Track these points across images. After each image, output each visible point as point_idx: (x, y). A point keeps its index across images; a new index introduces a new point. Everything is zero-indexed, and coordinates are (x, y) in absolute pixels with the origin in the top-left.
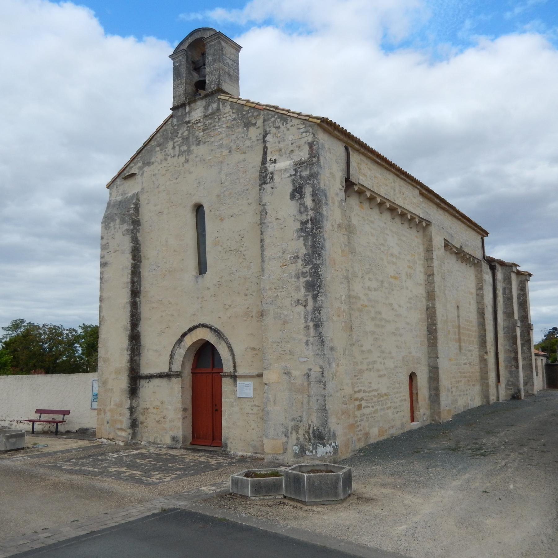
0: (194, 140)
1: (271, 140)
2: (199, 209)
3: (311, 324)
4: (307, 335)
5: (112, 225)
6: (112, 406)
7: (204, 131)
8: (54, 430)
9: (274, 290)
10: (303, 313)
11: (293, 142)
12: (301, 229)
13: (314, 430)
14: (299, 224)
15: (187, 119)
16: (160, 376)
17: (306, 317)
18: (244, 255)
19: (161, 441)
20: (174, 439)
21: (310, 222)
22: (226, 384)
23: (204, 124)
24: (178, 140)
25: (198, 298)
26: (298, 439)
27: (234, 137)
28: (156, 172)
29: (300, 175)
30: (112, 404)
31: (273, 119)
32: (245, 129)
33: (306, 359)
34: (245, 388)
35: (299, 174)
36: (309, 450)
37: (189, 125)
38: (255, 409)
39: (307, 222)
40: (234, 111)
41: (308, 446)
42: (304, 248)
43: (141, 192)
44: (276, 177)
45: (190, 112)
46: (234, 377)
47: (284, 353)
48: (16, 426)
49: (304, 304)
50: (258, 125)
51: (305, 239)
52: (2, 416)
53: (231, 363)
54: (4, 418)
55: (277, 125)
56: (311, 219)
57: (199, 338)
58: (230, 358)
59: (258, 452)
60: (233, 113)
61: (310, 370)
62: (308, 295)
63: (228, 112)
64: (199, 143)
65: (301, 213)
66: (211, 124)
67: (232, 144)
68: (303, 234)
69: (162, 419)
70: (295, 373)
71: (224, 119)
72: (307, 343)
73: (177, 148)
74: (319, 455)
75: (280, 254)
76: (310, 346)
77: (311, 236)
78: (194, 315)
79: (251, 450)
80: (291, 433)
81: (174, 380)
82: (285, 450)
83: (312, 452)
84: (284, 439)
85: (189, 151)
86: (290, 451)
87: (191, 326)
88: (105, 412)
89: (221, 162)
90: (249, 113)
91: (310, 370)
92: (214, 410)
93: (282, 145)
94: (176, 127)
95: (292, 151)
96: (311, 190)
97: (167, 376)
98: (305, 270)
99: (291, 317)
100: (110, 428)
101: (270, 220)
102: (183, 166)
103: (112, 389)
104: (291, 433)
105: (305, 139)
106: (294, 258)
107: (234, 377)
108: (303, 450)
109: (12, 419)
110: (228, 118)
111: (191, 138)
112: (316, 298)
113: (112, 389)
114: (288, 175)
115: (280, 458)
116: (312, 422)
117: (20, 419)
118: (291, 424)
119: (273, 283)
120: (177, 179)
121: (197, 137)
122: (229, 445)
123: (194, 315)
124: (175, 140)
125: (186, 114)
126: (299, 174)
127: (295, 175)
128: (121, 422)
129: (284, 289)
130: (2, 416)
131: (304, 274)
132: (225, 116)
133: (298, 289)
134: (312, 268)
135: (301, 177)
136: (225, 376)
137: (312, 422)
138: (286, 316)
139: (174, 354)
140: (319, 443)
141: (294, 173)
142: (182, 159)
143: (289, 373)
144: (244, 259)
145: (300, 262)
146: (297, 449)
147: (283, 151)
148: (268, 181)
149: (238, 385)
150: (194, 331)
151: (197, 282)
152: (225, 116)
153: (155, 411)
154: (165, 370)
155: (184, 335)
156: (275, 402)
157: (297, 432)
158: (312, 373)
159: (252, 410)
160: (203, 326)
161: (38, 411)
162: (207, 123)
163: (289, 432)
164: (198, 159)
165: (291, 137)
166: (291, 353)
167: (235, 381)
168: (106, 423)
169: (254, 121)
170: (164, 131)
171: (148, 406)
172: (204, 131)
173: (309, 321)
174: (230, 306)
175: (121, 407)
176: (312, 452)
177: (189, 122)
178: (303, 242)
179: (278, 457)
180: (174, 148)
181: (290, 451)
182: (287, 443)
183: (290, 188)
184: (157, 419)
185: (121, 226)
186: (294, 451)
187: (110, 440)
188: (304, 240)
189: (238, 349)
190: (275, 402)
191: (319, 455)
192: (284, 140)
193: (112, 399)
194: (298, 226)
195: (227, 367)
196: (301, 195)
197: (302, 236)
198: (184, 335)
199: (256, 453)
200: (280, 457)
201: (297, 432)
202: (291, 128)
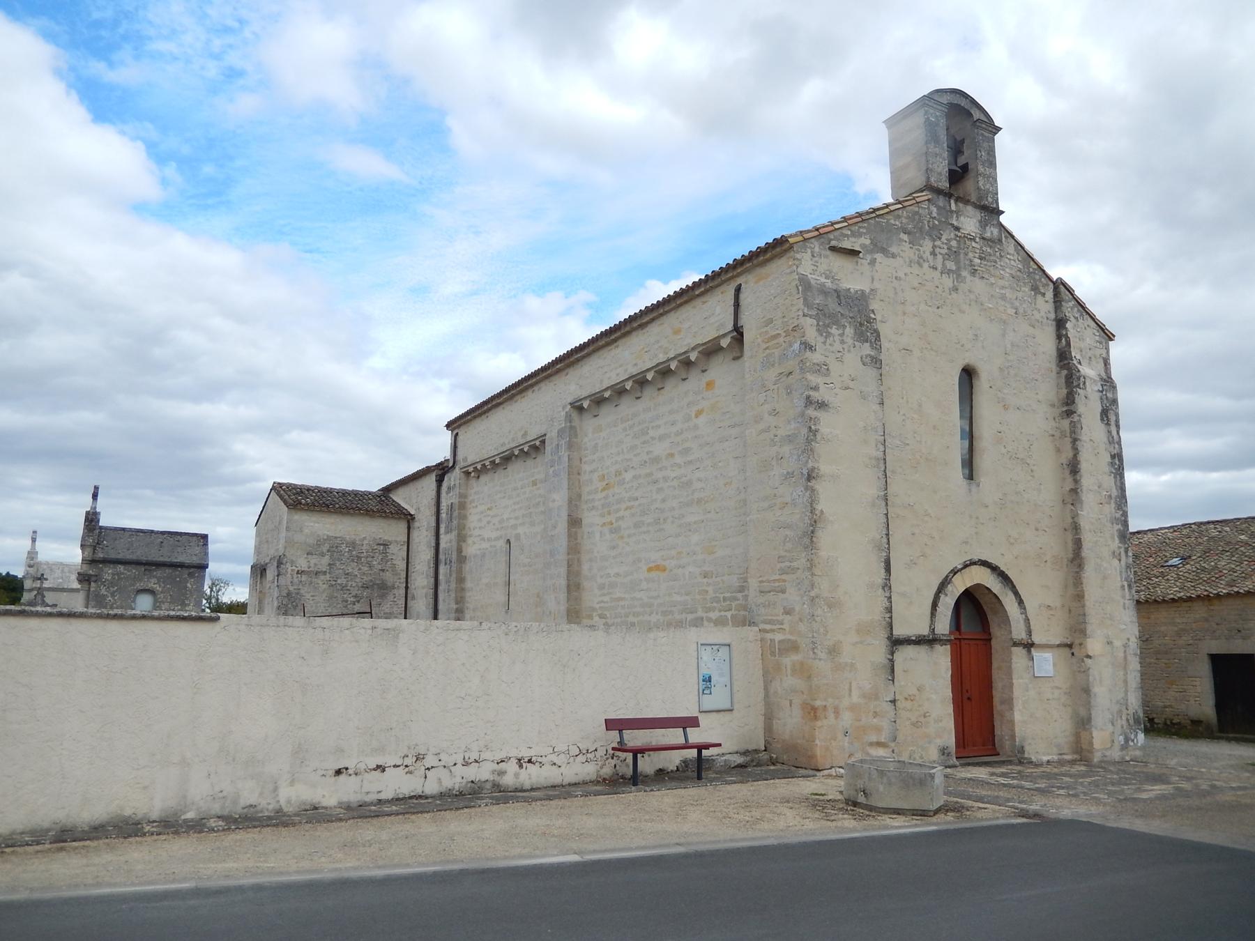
2: (968, 374)
3: (1126, 584)
4: (1123, 597)
5: (834, 330)
6: (855, 698)
8: (630, 772)
16: (919, 641)
19: (921, 757)
20: (943, 751)
25: (971, 517)
28: (901, 274)
30: (855, 693)
34: (1045, 662)
38: (1057, 692)
46: (1029, 646)
48: (517, 775)
52: (468, 749)
53: (1022, 625)
54: (474, 756)
69: (922, 719)
78: (966, 543)
79: (1055, 750)
85: (957, 274)
88: (837, 712)
92: (965, 697)
100: (851, 743)
103: (852, 665)
107: (1029, 646)
109: (502, 755)
113: (852, 665)
117: (526, 754)
122: (1027, 748)
128: (878, 730)
130: (468, 749)
153: (908, 704)
154: (924, 630)
160: (984, 563)
161: (611, 724)
164: (972, 297)
168: (840, 736)
174: (1016, 540)
175: (877, 698)
181: (1116, 743)
183: (1100, 409)
184: (914, 719)
189: (1035, 605)
193: (854, 684)
195: (1019, 632)
198: (955, 572)
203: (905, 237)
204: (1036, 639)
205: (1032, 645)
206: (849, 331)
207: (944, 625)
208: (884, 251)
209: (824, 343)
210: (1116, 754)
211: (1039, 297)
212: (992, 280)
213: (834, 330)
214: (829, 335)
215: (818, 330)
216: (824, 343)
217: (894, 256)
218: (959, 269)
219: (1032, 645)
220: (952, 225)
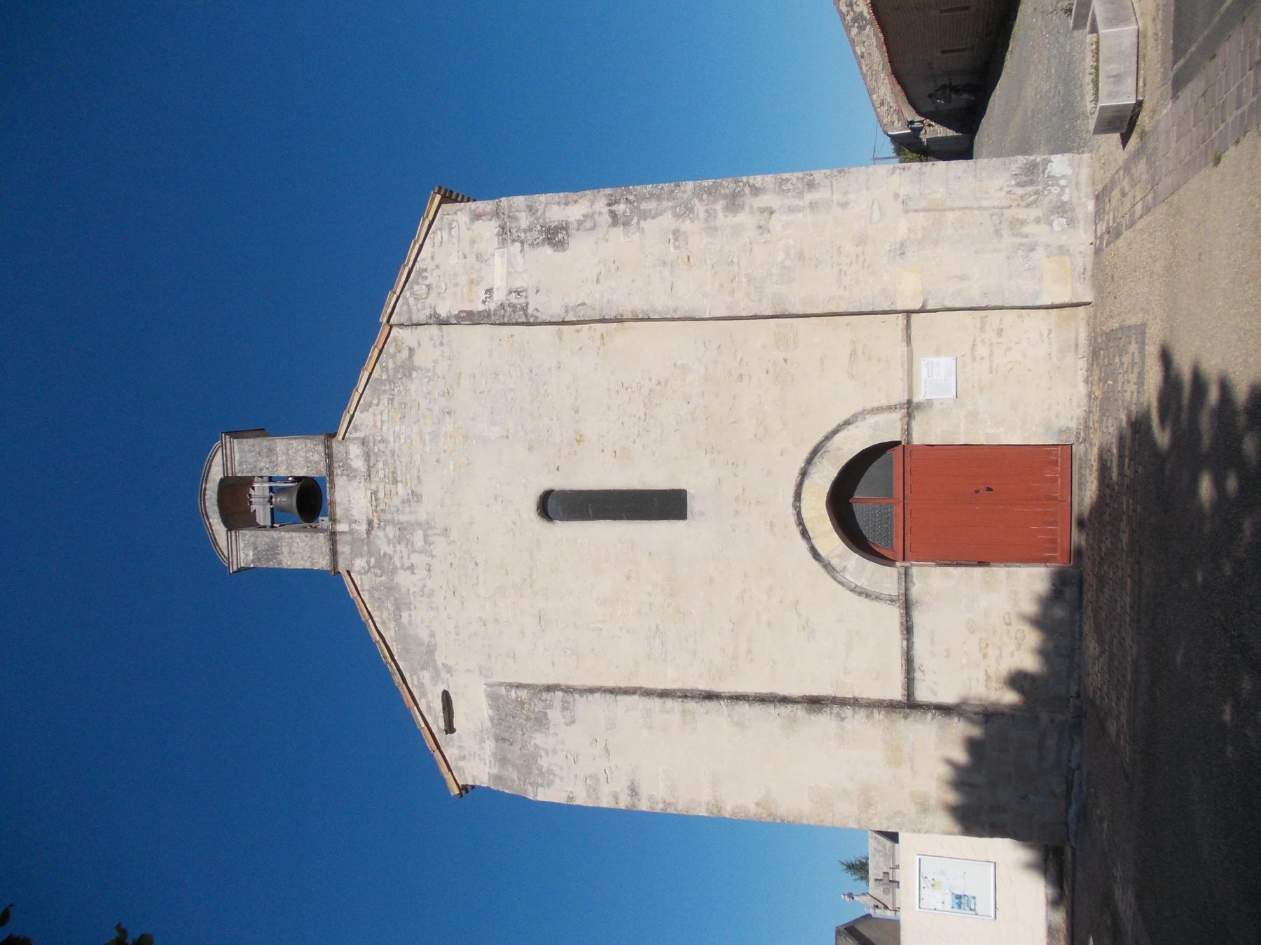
0: (408, 509)
1: (448, 304)
7: (395, 482)
9: (735, 284)
10: (784, 217)
11: (461, 256)
12: (625, 224)
13: (1019, 185)
14: (615, 229)
15: (363, 528)
17: (792, 210)
18: (659, 383)
21: (613, 208)
22: (927, 433)
23: (382, 480)
24: (399, 554)
25: (737, 513)
26: (1038, 220)
27: (424, 404)
29: (525, 231)
31: (411, 301)
32: (414, 374)
33: (876, 206)
34: (936, 377)
35: (522, 235)
36: (1060, 195)
37: (376, 522)
39: (613, 215)
40: (375, 402)
41: (1050, 197)
42: (660, 218)
43: (486, 677)
44: (519, 283)
45: (352, 521)
47: (861, 259)
49: (766, 215)
50: (414, 344)
51: (644, 215)
55: (424, 289)
56: (609, 205)
57: (824, 512)
58: (872, 419)
59: (1073, 342)
60: (378, 404)
61: (896, 196)
62: (751, 207)
63: (375, 415)
64: (415, 496)
65: (594, 227)
66: (386, 463)
67: (436, 409)
68: (634, 221)
70: (902, 231)
71: (385, 428)
72: (844, 205)
73: (415, 558)
74: (1069, 172)
75: (666, 271)
76: (851, 196)
77: (639, 203)
80: (1027, 236)
81: (915, 592)
82: (1063, 250)
83: (1063, 188)
84: (1040, 253)
85: (427, 526)
86: (1064, 238)
87: (796, 531)
89: (466, 437)
90: (386, 367)
91: (896, 196)
93: (463, 279)
94: (373, 560)
95: (479, 257)
96: (555, 208)
97: (907, 605)
98: (702, 215)
99: (791, 242)
101: (597, 296)
102: (454, 542)
104: (1027, 236)
105: (463, 228)
106: (676, 240)
107: (910, 408)
108: (1062, 209)
110: (385, 417)
111: (403, 518)
112: (757, 189)
114: (519, 259)
115: (1081, 264)
116: (1001, 189)
118: (1008, 239)
119: (722, 286)
120: (476, 564)
121: (403, 502)
123: (772, 525)
124: (398, 564)
125: (351, 532)
126: (522, 235)
127: (522, 242)
129: (735, 260)
131: (710, 214)
132: (379, 424)
133: (737, 230)
134: (701, 200)
135: (529, 230)
136: (908, 431)
137: (1001, 189)
138: (788, 255)
139: (856, 586)
140: (1043, 172)
141: (518, 245)
142: (440, 546)
143: (902, 245)
144: (666, 382)
145: (686, 226)
146: (1059, 222)
147: (474, 276)
148: (522, 300)
149: (928, 397)
150: (808, 525)
151: (702, 514)
152: (379, 424)
154: (894, 614)
155: (816, 554)
156: (963, 278)
157: (1023, 223)
158: (903, 192)
159: (982, 358)
162: (381, 473)
163: (1024, 241)
165: (453, 260)
166: (861, 241)
167: (919, 406)
169: (405, 354)
170: (372, 596)
171: (982, 677)
172: (395, 482)
173: (801, 203)
176: (1063, 188)
177: (370, 523)
178: (649, 220)
179: (1079, 269)
180: (412, 568)
182: (1047, 246)
183: (548, 250)
185: (552, 730)
186: (1063, 230)
187: (1069, 788)
188: (645, 219)
189: (849, 399)
190: (963, 278)
191: (1069, 172)
192: (455, 275)
194: (619, 230)
195: (887, 429)
196: (562, 228)
197: (638, 223)
198: (816, 554)
199: (1077, 345)
200: (1080, 261)
201: (1023, 223)
202: (437, 261)
203: (405, 615)
204: (899, 396)
205: (909, 402)
206: (539, 739)
207: (884, 578)
208: (431, 650)
209: (561, 779)
210: (1082, 239)
211: (419, 359)
212: (417, 458)
213: (544, 762)
214: (550, 771)
215: (549, 786)
216: (561, 779)
217: (432, 635)
218: (419, 524)
219: (909, 402)
220: (369, 532)
